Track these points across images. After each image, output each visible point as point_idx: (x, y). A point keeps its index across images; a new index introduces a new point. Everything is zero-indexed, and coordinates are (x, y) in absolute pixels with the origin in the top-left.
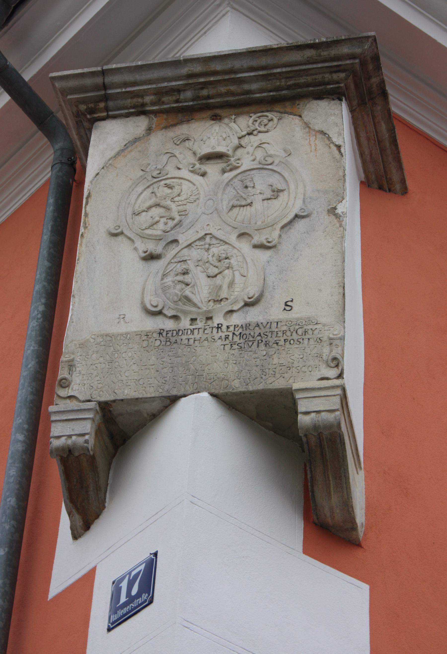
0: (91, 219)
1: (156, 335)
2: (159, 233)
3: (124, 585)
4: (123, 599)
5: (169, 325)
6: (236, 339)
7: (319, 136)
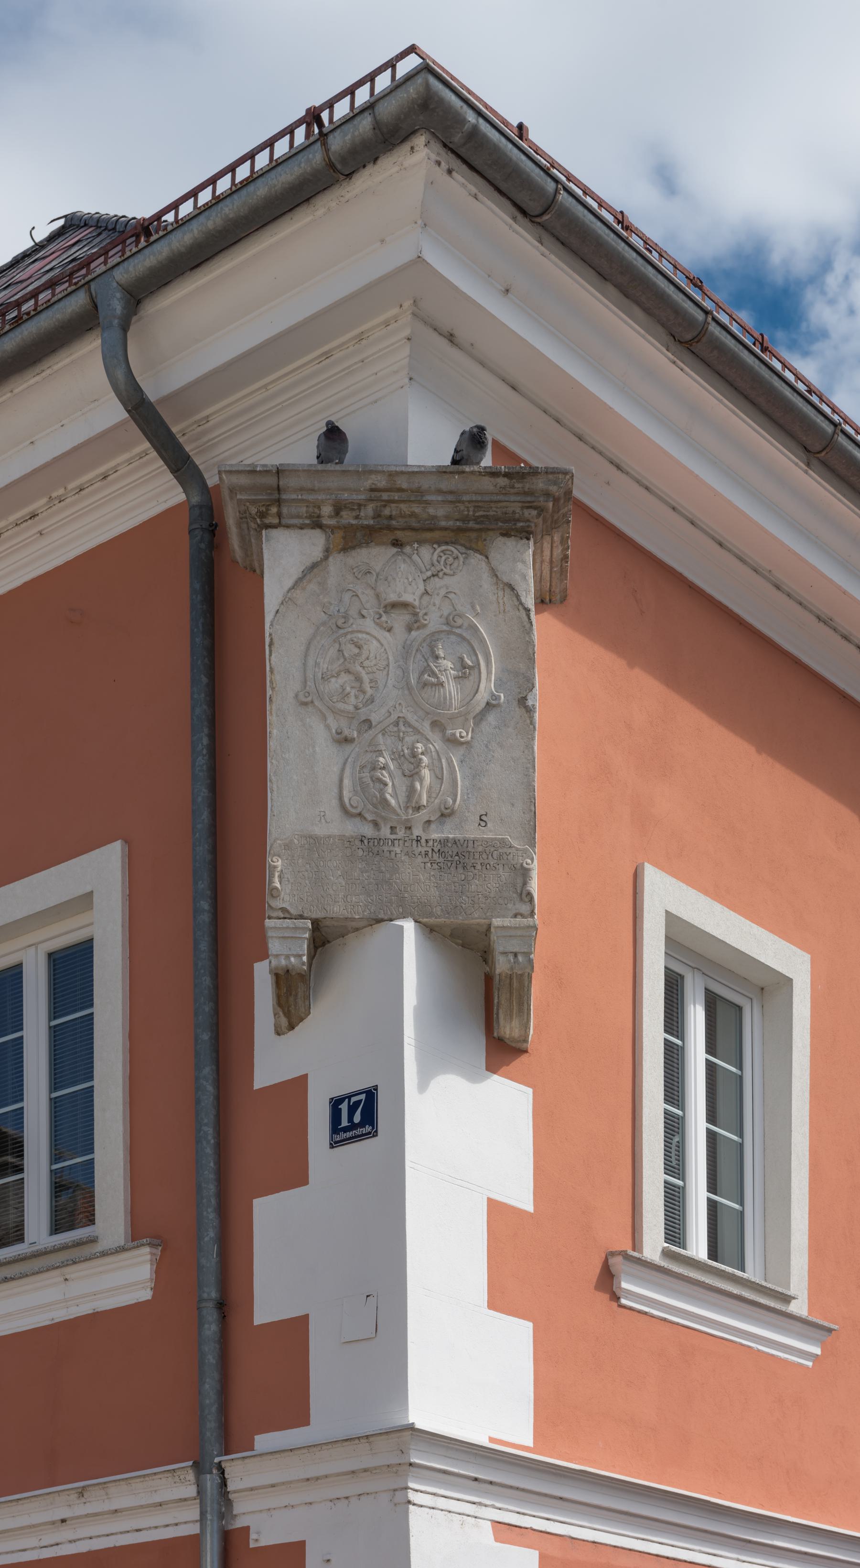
0: (277, 677)
1: (358, 843)
2: (351, 708)
3: (344, 1107)
4: (345, 1123)
5: (368, 831)
6: (436, 856)
7: (508, 591)
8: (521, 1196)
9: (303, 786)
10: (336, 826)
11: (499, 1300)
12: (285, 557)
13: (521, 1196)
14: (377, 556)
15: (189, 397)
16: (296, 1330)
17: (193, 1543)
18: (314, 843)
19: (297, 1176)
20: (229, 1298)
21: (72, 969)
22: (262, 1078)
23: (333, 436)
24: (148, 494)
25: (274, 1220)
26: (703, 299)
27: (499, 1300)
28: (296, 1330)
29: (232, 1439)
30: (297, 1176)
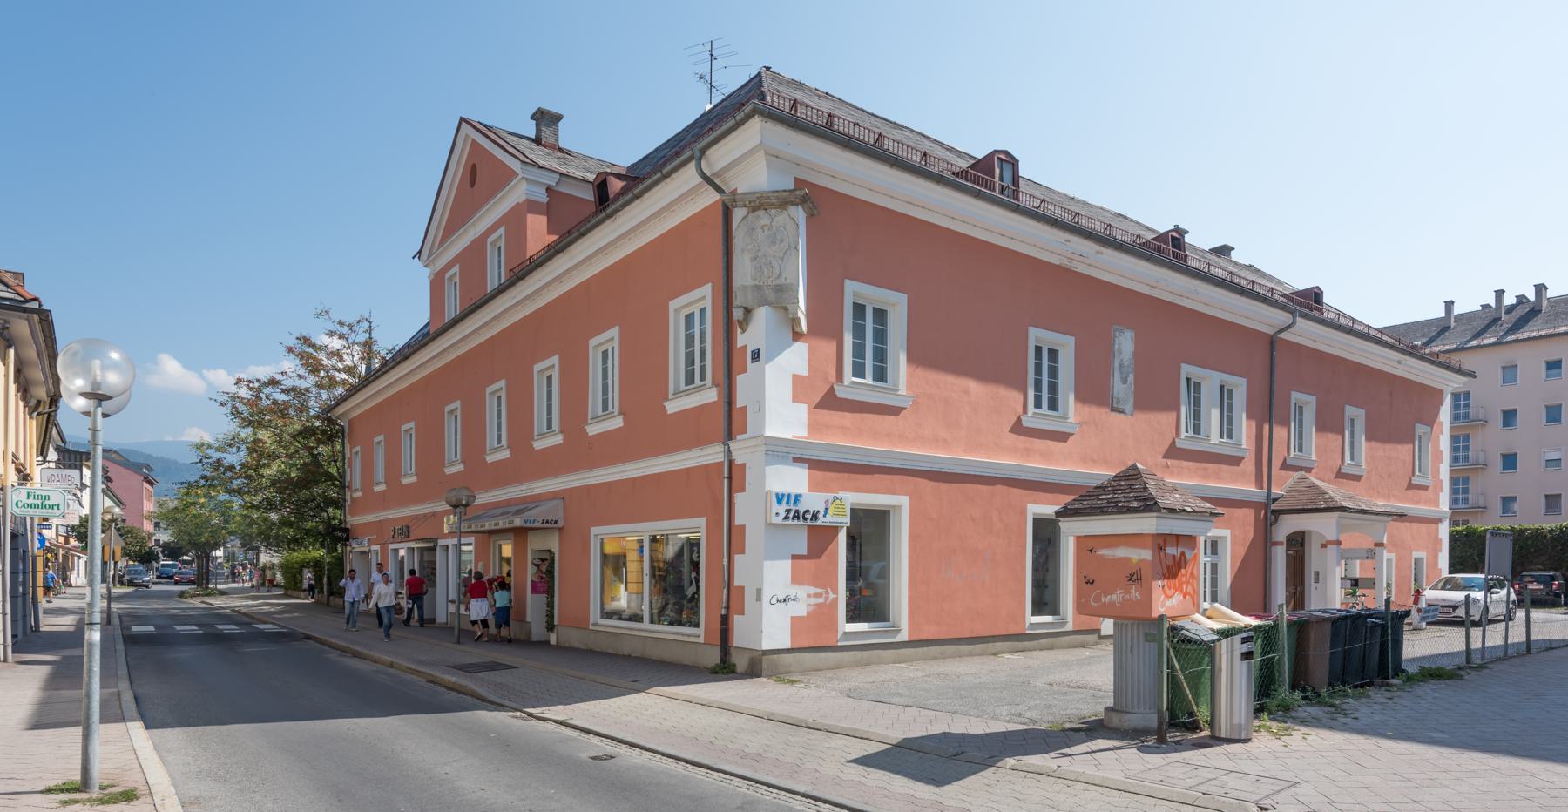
8: (804, 372)
9: (744, 273)
10: (750, 282)
11: (796, 399)
12: (738, 214)
13: (804, 372)
14: (761, 213)
15: (716, 174)
16: (744, 409)
17: (721, 464)
18: (745, 287)
19: (744, 370)
20: (730, 401)
21: (702, 311)
22: (739, 344)
23: (546, 119)
24: (711, 197)
25: (741, 380)
26: (1098, 765)
27: (796, 399)
28: (744, 409)
29: (730, 436)
30: (744, 370)
